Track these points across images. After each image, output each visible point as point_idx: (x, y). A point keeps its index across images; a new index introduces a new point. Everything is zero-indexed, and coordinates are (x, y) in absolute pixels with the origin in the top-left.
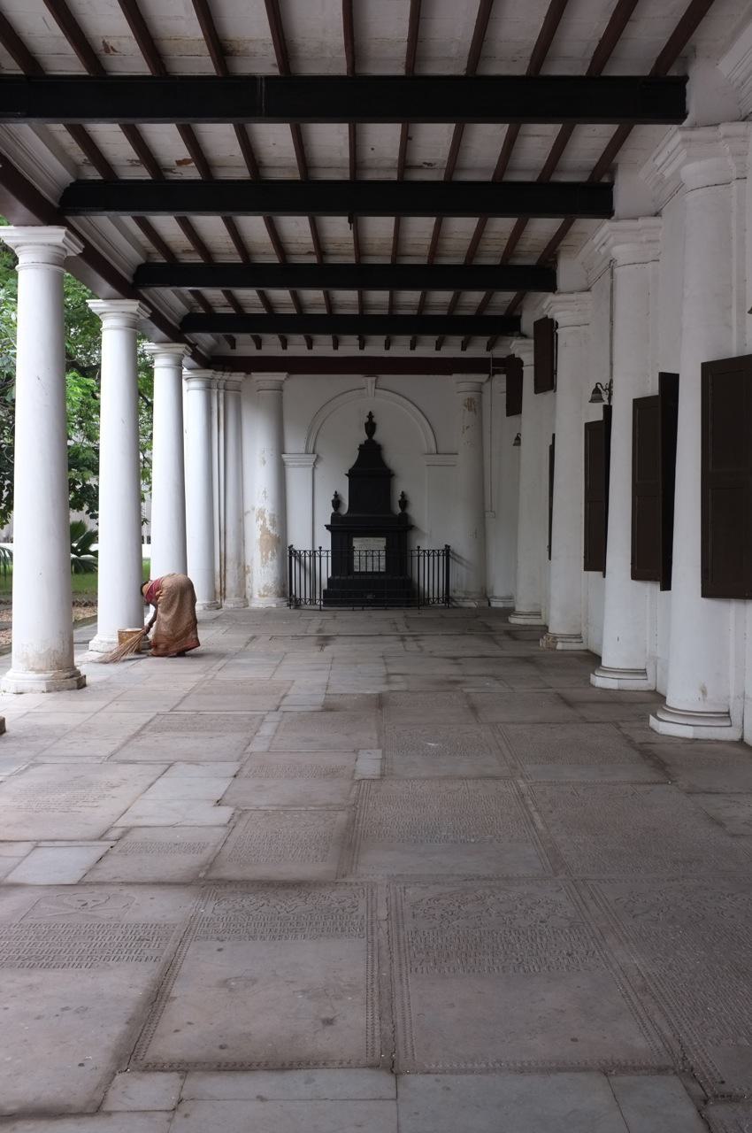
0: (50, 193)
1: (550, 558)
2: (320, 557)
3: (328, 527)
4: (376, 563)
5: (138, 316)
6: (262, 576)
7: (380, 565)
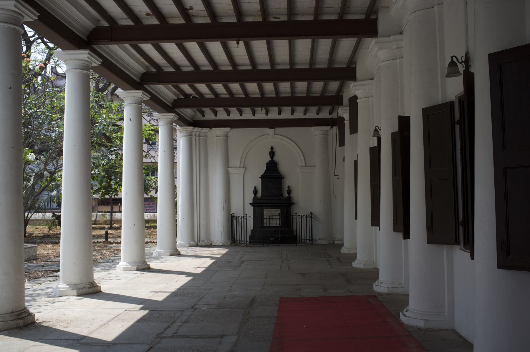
1: (356, 219)
4: (274, 222)
7: (277, 222)
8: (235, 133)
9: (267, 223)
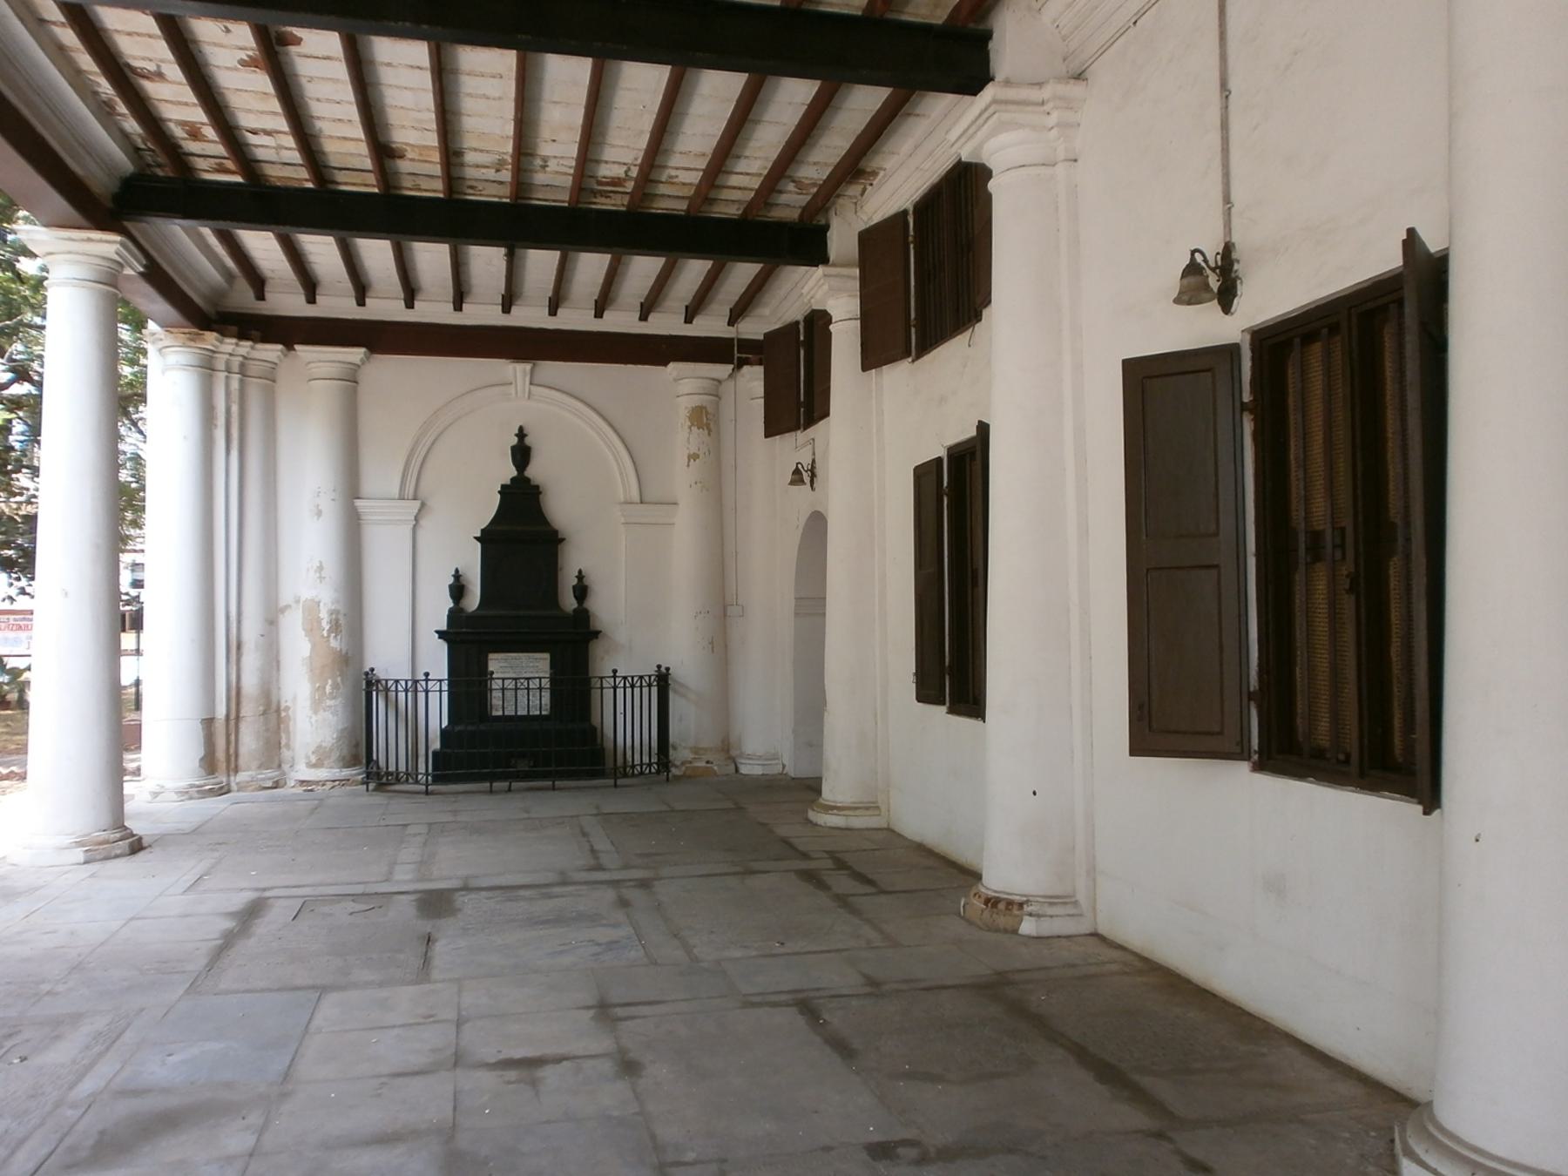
0: (101, 183)
2: (427, 692)
3: (441, 634)
4: (535, 701)
5: (121, 265)
6: (313, 725)
7: (538, 703)
8: (400, 378)
9: (500, 705)
